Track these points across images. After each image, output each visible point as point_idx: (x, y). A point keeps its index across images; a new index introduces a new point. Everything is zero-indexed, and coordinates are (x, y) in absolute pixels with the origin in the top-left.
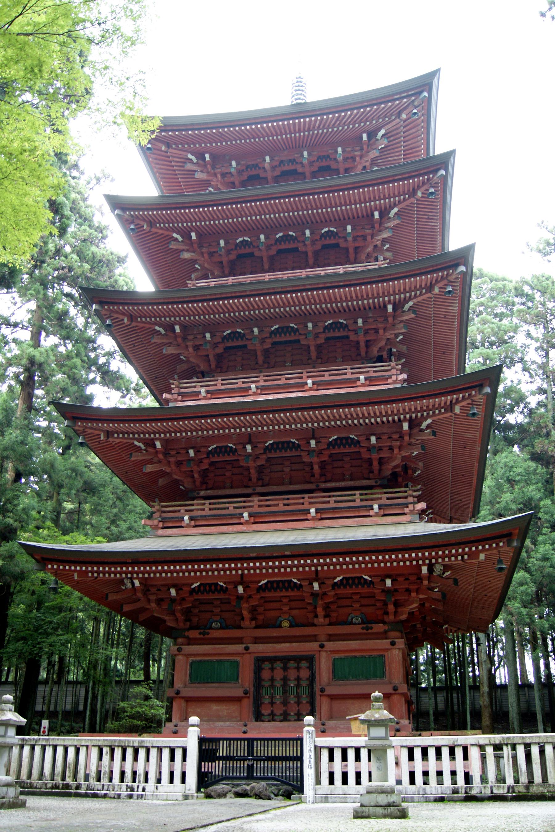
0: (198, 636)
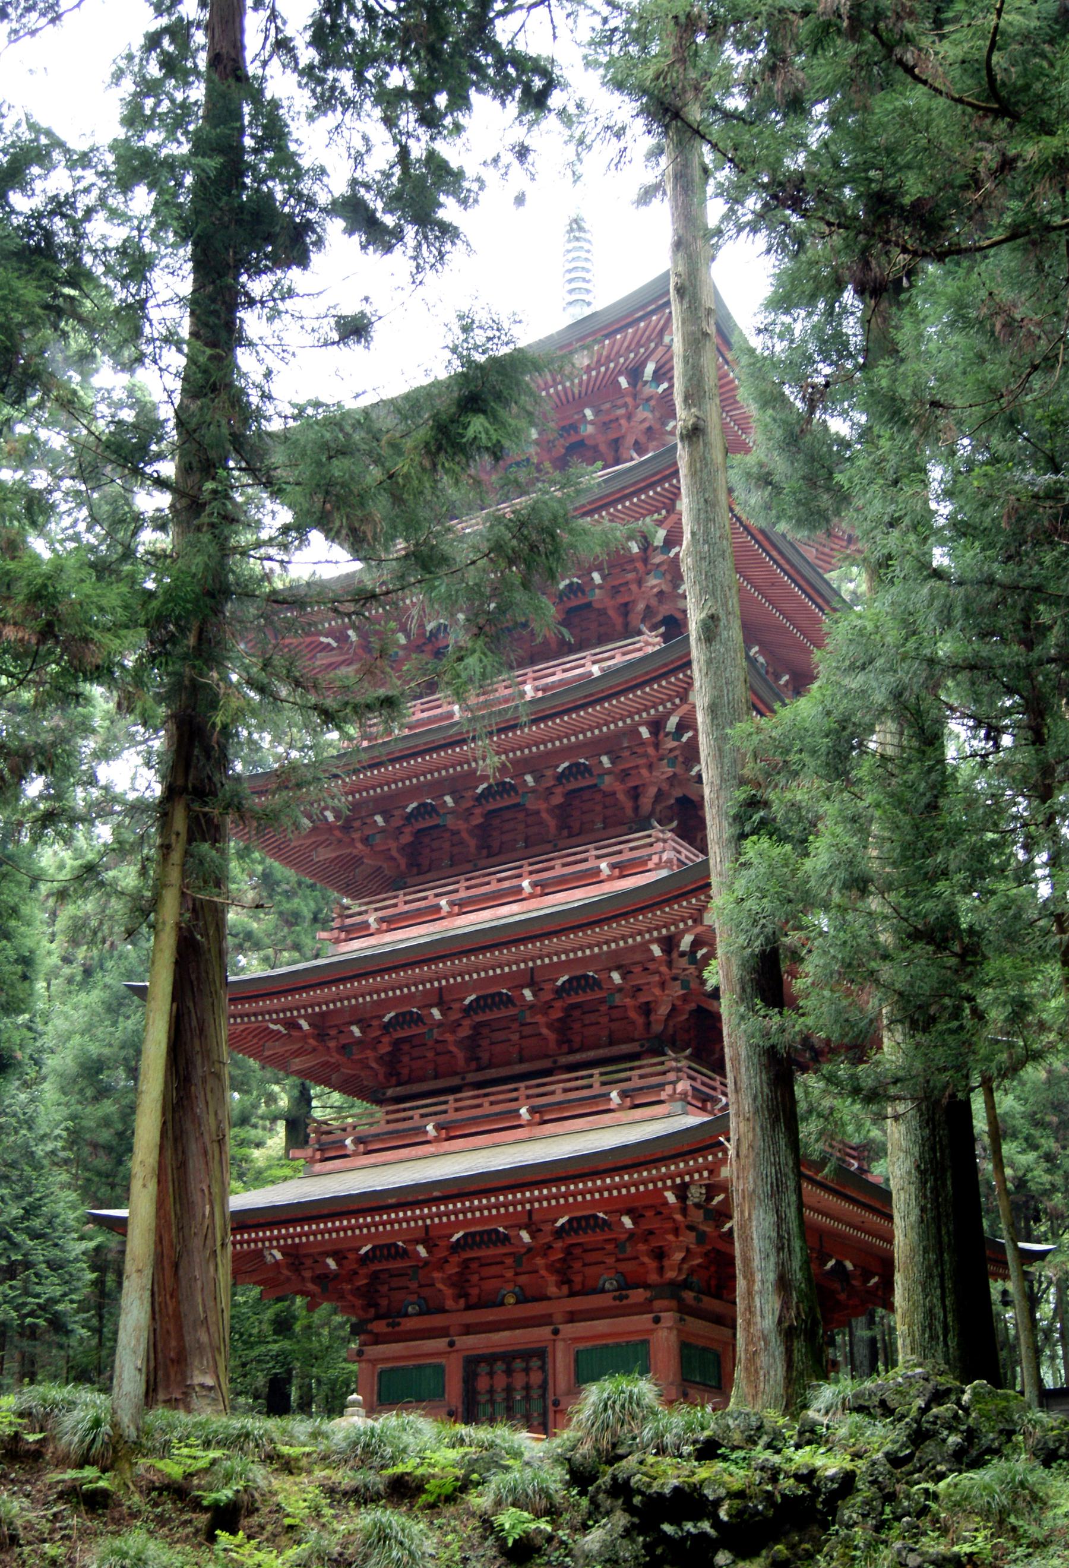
0: (386, 1330)
